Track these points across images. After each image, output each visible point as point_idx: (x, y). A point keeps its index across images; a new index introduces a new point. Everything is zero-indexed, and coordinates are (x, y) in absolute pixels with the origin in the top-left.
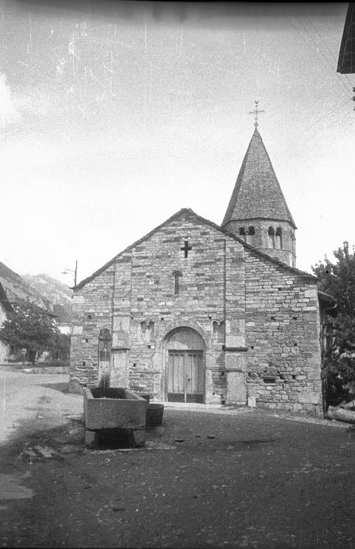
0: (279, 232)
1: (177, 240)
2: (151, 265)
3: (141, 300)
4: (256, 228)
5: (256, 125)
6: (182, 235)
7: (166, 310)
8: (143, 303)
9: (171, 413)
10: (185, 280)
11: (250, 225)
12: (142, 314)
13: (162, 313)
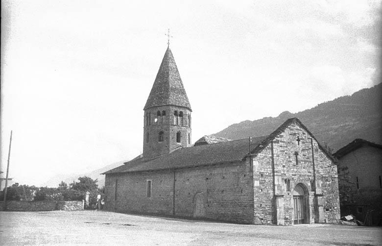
0: (181, 115)
1: (295, 134)
2: (286, 147)
3: (284, 166)
4: (184, 113)
5: (168, 43)
6: (296, 132)
7: (294, 173)
8: (285, 169)
9: (72, 208)
10: (300, 157)
11: (181, 110)
12: (285, 174)
13: (293, 175)
